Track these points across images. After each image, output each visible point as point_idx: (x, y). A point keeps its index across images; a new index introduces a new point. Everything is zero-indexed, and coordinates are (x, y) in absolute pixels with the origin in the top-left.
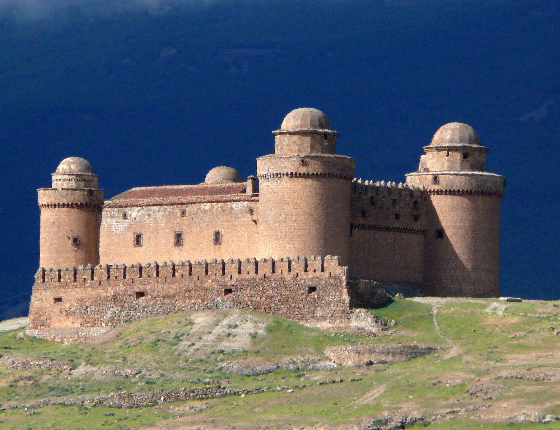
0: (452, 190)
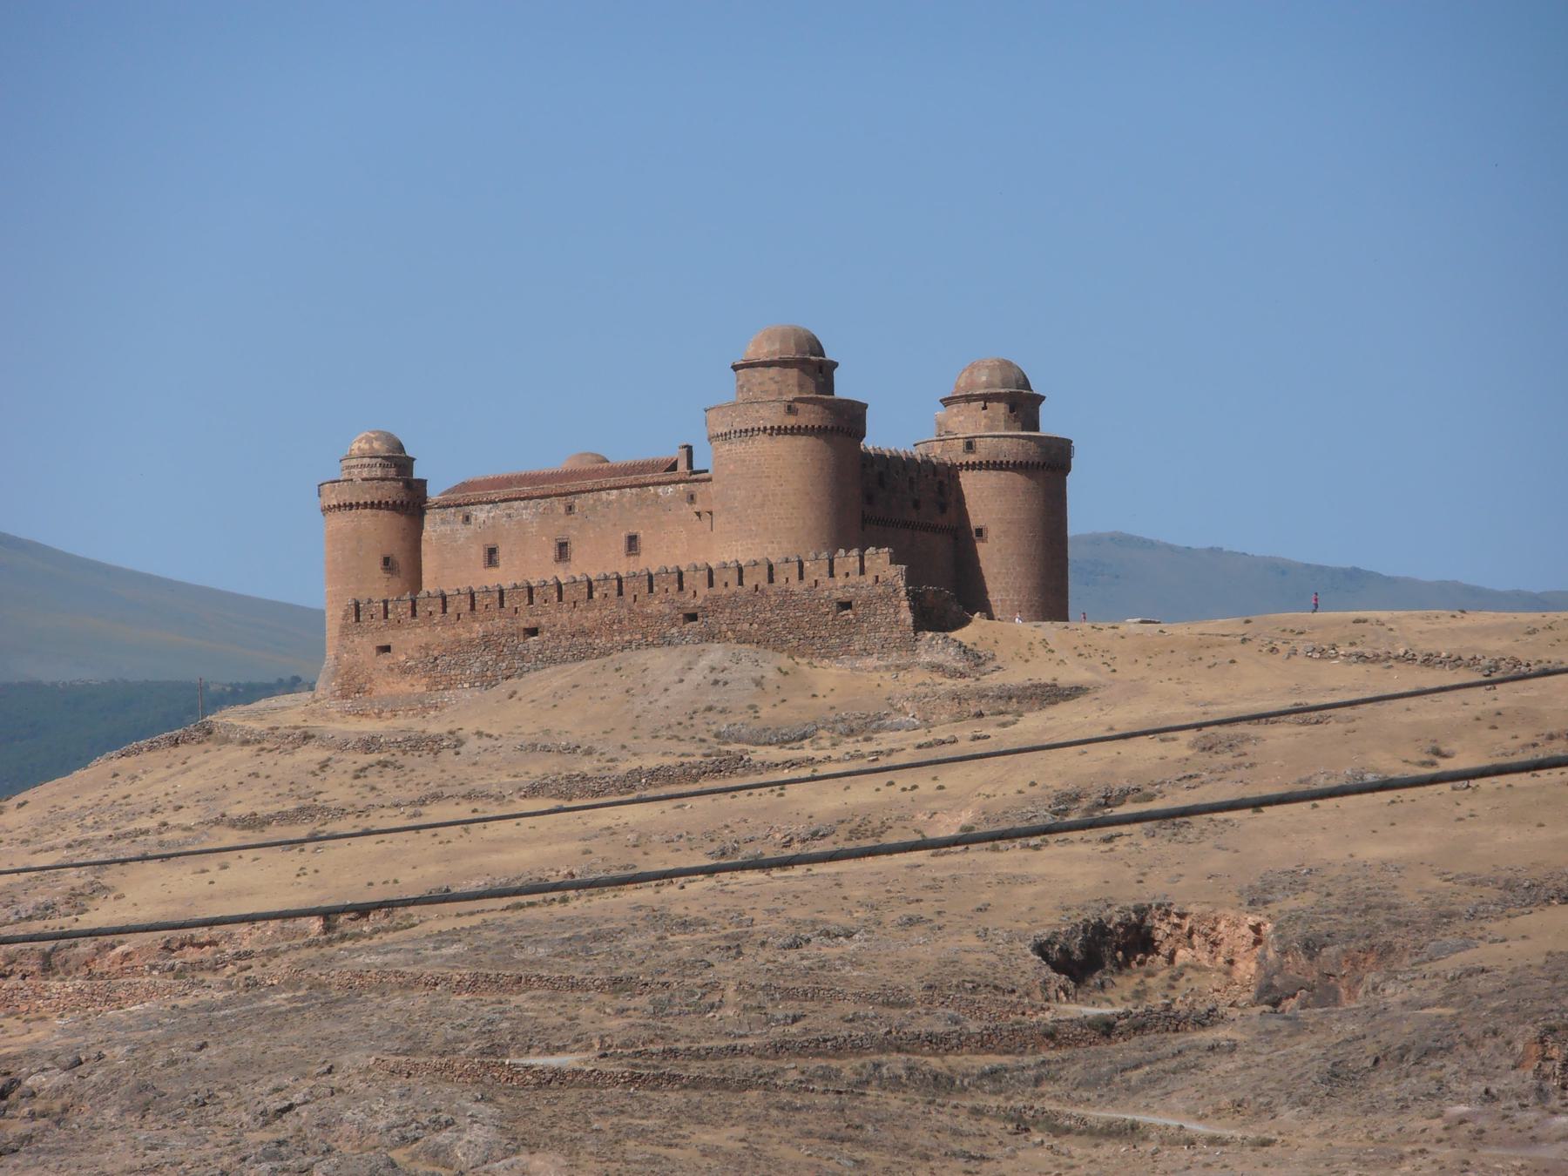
0: (998, 462)
